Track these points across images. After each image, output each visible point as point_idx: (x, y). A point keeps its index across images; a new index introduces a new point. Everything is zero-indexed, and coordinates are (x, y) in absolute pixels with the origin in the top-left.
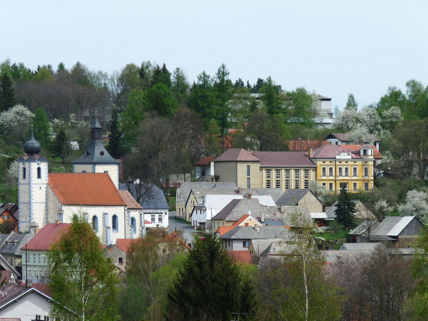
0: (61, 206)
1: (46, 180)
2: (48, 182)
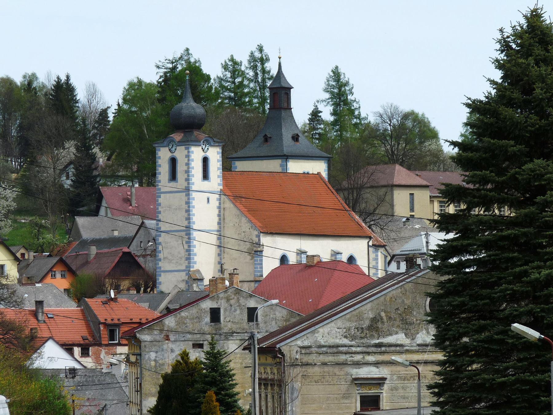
0: (258, 236)
1: (219, 185)
2: (221, 187)
